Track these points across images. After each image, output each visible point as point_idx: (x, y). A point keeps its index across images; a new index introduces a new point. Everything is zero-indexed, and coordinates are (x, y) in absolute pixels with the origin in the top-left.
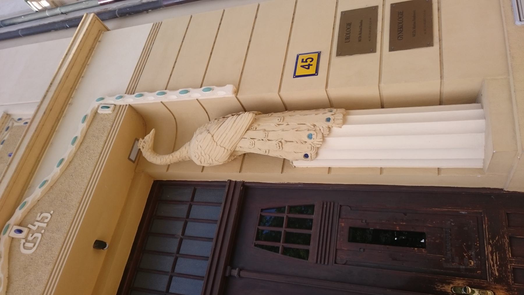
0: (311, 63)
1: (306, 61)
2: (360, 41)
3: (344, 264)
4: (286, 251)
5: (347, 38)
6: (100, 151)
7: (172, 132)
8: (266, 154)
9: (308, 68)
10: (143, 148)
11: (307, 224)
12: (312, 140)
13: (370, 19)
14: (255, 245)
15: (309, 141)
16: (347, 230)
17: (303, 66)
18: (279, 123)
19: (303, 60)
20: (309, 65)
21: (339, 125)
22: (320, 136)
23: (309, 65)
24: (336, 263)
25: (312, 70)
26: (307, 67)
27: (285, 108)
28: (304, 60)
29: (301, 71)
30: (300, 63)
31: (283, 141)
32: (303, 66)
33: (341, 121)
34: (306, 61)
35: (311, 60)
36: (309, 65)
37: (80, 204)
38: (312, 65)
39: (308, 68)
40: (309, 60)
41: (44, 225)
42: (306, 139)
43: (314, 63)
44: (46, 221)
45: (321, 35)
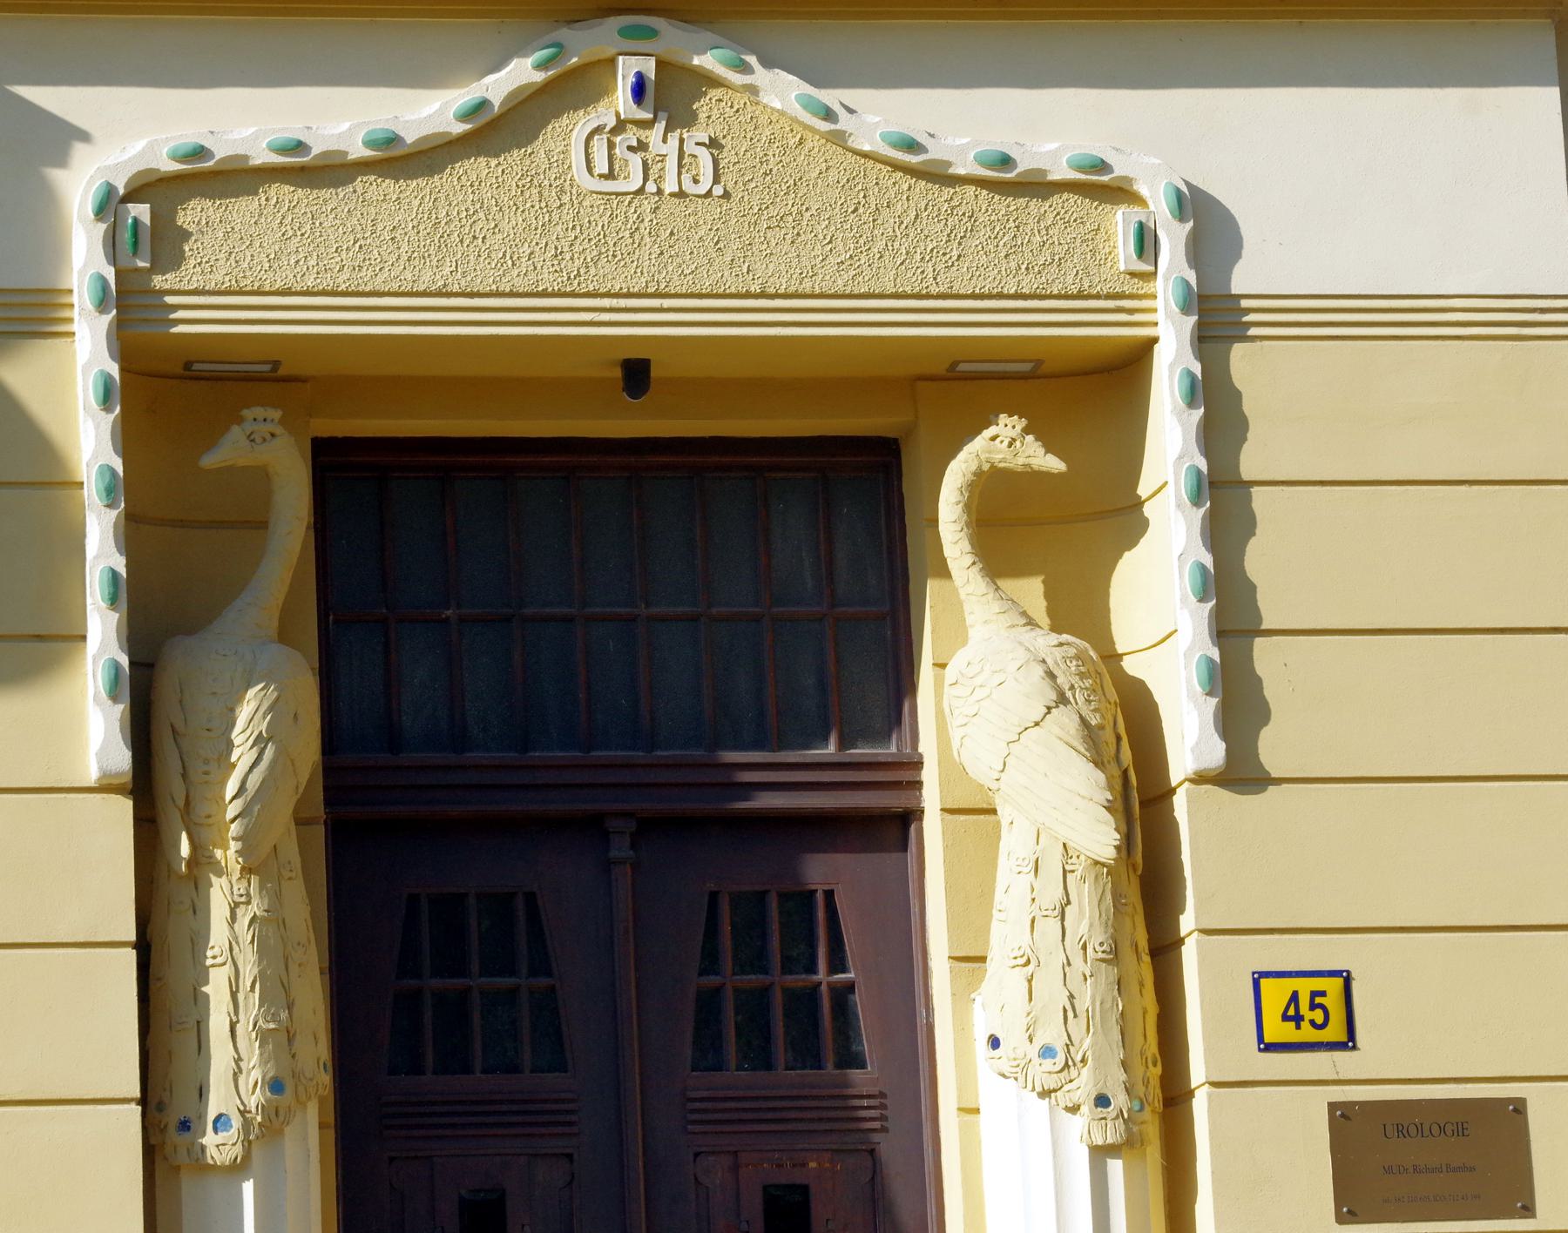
0: (1305, 1025)
1: (1313, 1007)
2: (1388, 1170)
3: (1061, 1071)
4: (708, 1005)
5: (1402, 1131)
6: (958, 288)
7: (1062, 538)
8: (994, 912)
9: (1285, 1018)
10: (993, 439)
11: (807, 1054)
12: (1036, 1061)
13: (1477, 1197)
14: (714, 896)
15: (1033, 1052)
16: (798, 1178)
17: (1295, 997)
18: (1090, 950)
19: (1323, 994)
20: (1298, 1019)
21: (1086, 1135)
22: (1051, 1083)
23: (1320, 1015)
24: (697, 1155)
25: (1277, 1030)
26: (1291, 1012)
27: (1164, 951)
28: (1318, 1000)
29: (1275, 994)
30: (1305, 987)
31: (1031, 968)
32: (1295, 997)
33: (1100, 1143)
34: (1313, 1007)
35: (1320, 1021)
36: (1298, 1019)
37: (763, 295)
38: (1298, 1027)
39: (1285, 1018)
40: (1318, 1016)
41: (670, 186)
42: (1039, 1041)
43: (1307, 1034)
44: (688, 186)
45: (1413, 1046)
